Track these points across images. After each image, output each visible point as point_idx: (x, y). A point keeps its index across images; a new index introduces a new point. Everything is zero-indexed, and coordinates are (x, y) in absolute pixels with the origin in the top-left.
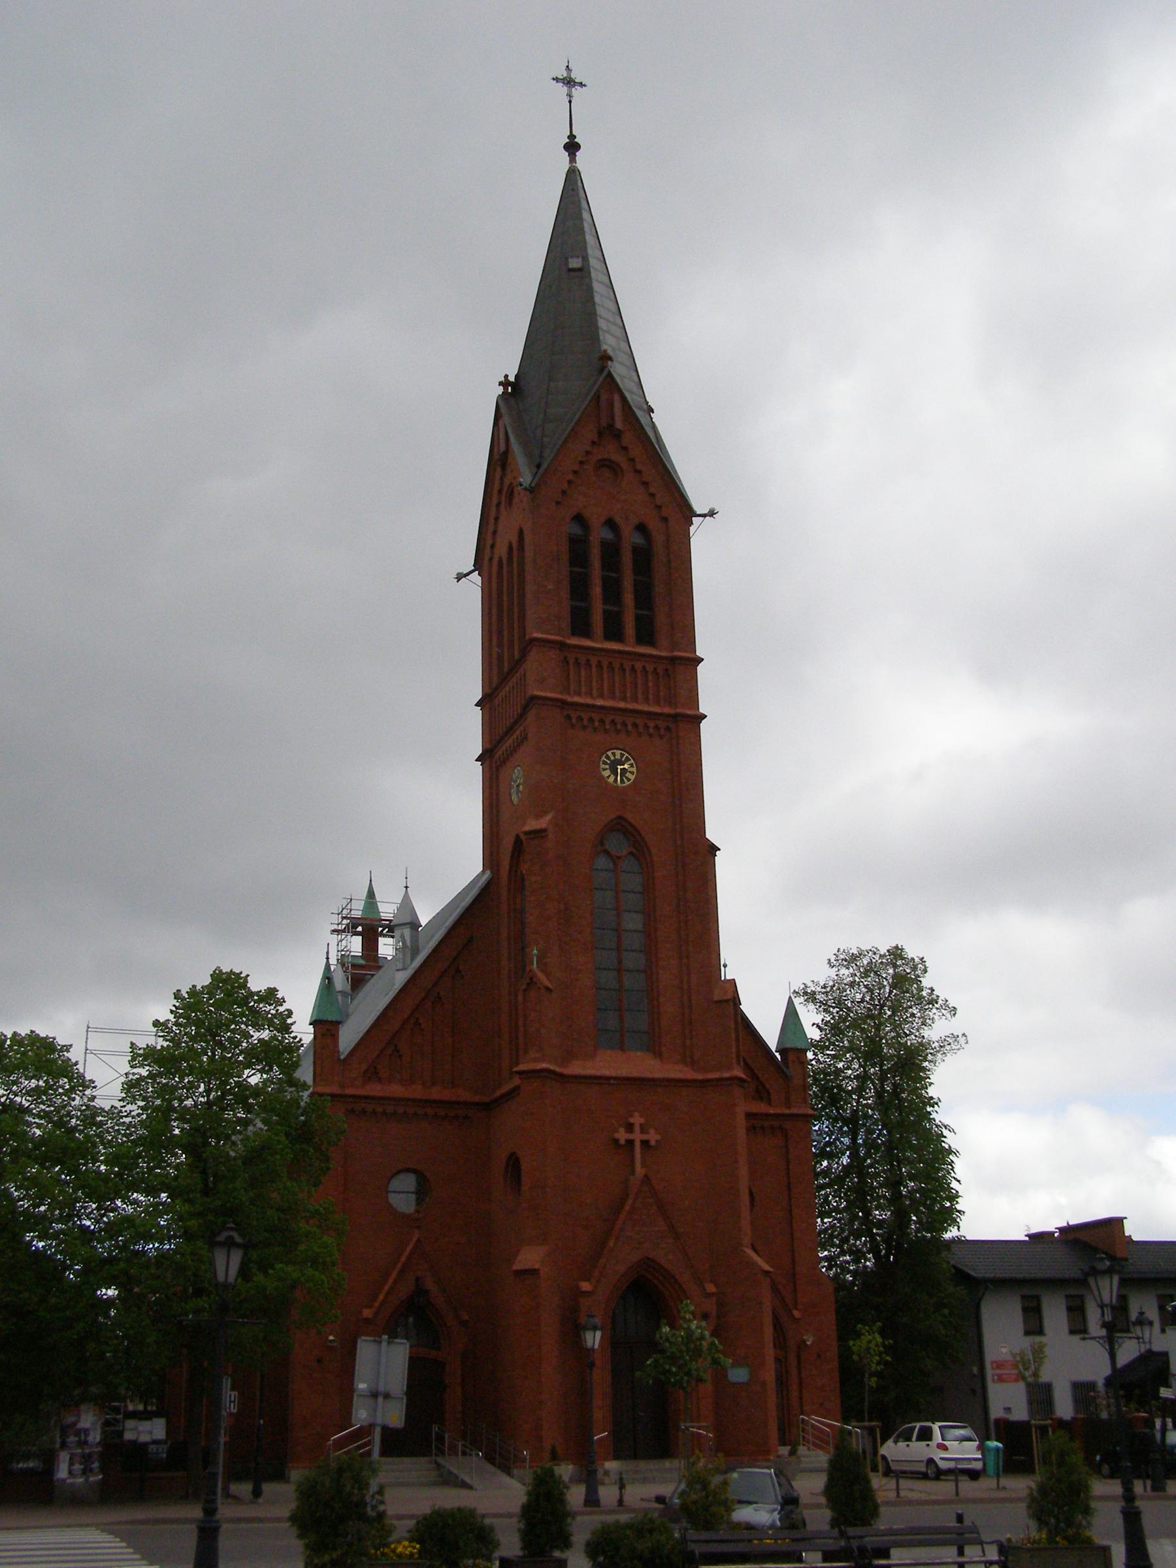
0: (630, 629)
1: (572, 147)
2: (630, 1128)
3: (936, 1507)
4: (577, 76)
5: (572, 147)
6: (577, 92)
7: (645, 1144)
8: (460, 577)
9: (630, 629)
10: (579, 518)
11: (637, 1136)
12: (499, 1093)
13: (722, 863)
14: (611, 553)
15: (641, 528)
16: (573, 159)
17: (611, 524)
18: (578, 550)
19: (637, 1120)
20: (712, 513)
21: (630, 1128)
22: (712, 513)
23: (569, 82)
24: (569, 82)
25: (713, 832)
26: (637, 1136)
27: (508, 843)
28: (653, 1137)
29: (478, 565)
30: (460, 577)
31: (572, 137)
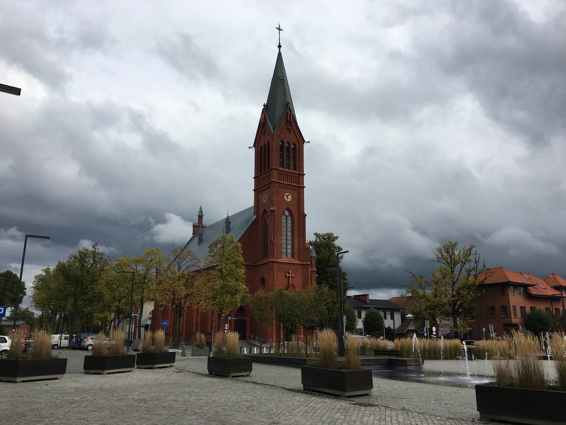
0: (292, 168)
1: (280, 46)
2: (289, 273)
3: (455, 389)
4: (281, 28)
5: (280, 46)
6: (281, 32)
7: (292, 277)
8: (250, 148)
9: (292, 168)
10: (282, 141)
11: (290, 275)
12: (260, 263)
13: (307, 218)
14: (288, 148)
15: (294, 144)
16: (280, 49)
17: (288, 143)
18: (282, 147)
19: (290, 272)
20: (309, 142)
21: (289, 273)
22: (309, 142)
23: (279, 29)
24: (279, 29)
25: (306, 212)
26: (290, 275)
27: (261, 210)
28: (293, 275)
29: (254, 146)
30: (250, 148)
31: (280, 44)
